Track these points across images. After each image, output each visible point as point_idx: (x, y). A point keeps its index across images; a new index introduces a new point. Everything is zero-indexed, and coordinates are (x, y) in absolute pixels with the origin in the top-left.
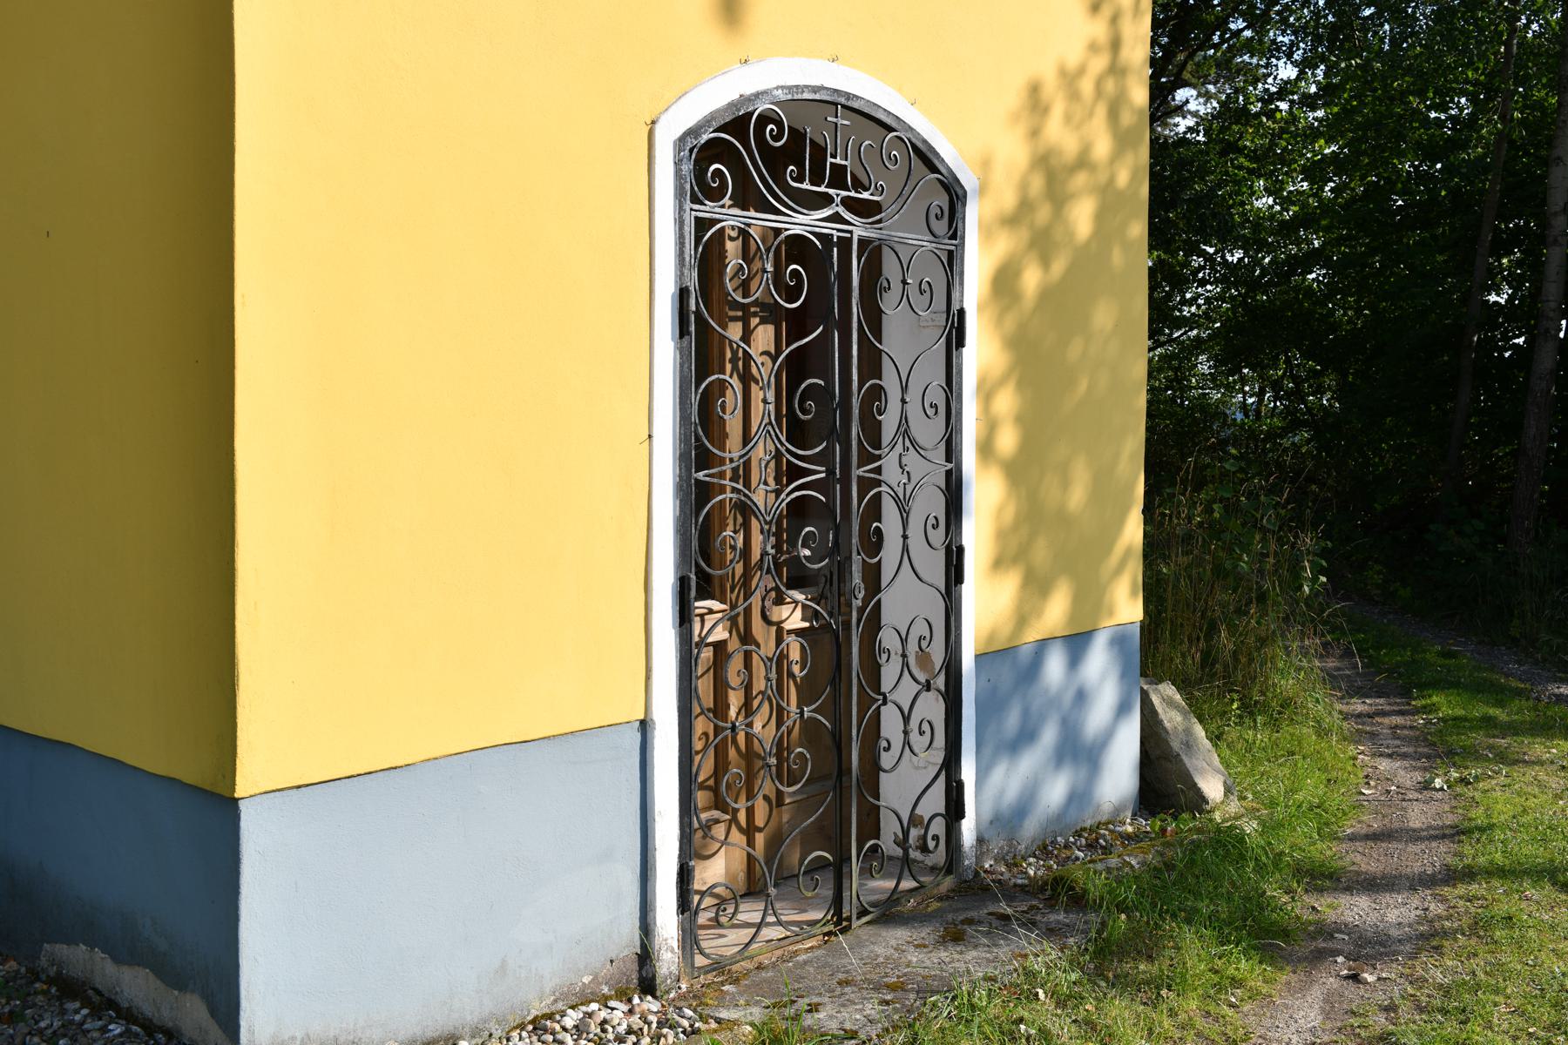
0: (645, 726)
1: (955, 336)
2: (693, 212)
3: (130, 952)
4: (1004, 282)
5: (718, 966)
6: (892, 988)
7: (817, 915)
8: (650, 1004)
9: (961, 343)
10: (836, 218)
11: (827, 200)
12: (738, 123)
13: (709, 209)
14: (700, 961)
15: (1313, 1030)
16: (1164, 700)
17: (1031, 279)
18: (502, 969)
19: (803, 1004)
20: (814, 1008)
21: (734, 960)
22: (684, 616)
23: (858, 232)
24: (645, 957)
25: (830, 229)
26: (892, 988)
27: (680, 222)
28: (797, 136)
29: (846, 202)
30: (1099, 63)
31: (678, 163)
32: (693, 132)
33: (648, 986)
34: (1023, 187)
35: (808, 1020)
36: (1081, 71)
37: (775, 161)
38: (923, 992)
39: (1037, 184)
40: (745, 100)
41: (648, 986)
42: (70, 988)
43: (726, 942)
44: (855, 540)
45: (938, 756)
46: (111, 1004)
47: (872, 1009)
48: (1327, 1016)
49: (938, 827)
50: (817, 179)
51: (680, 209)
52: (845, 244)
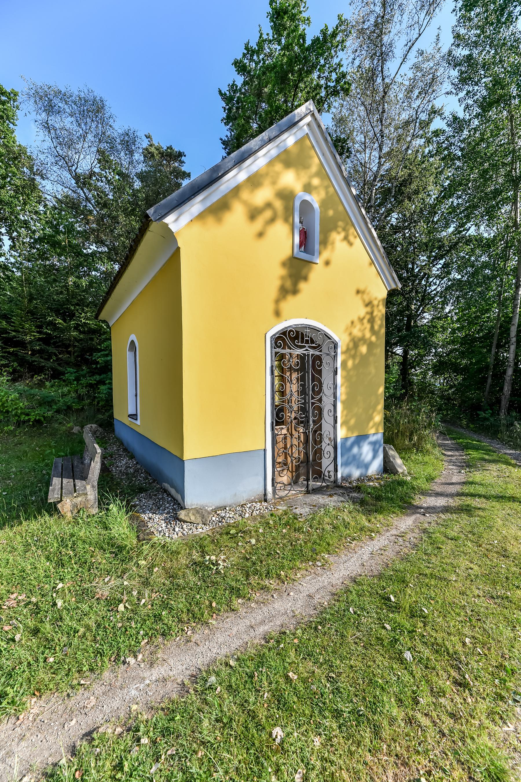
0: (265, 450)
1: (336, 373)
2: (274, 351)
3: (172, 486)
4: (344, 364)
5: (281, 498)
6: (313, 506)
7: (303, 489)
8: (266, 504)
9: (336, 374)
10: (307, 350)
11: (305, 347)
12: (284, 333)
13: (278, 350)
14: (277, 496)
15: (409, 526)
16: (444, 434)
17: (350, 363)
18: (235, 495)
19: (294, 507)
20: (296, 508)
21: (284, 497)
22: (273, 429)
23: (311, 353)
24: (265, 495)
25: (305, 352)
26: (313, 506)
27: (272, 353)
28: (297, 332)
29: (309, 347)
30: (368, 317)
31: (271, 341)
32: (274, 335)
33: (266, 501)
34: (348, 345)
35: (294, 511)
36: (364, 318)
37: (293, 339)
38: (320, 507)
39: (351, 345)
40: (286, 328)
41: (266, 501)
42: (165, 491)
43: (282, 493)
44: (311, 415)
45: (332, 458)
46: (170, 494)
47: (307, 510)
48: (414, 522)
49: (332, 474)
50: (302, 342)
51: (272, 350)
52: (308, 355)
